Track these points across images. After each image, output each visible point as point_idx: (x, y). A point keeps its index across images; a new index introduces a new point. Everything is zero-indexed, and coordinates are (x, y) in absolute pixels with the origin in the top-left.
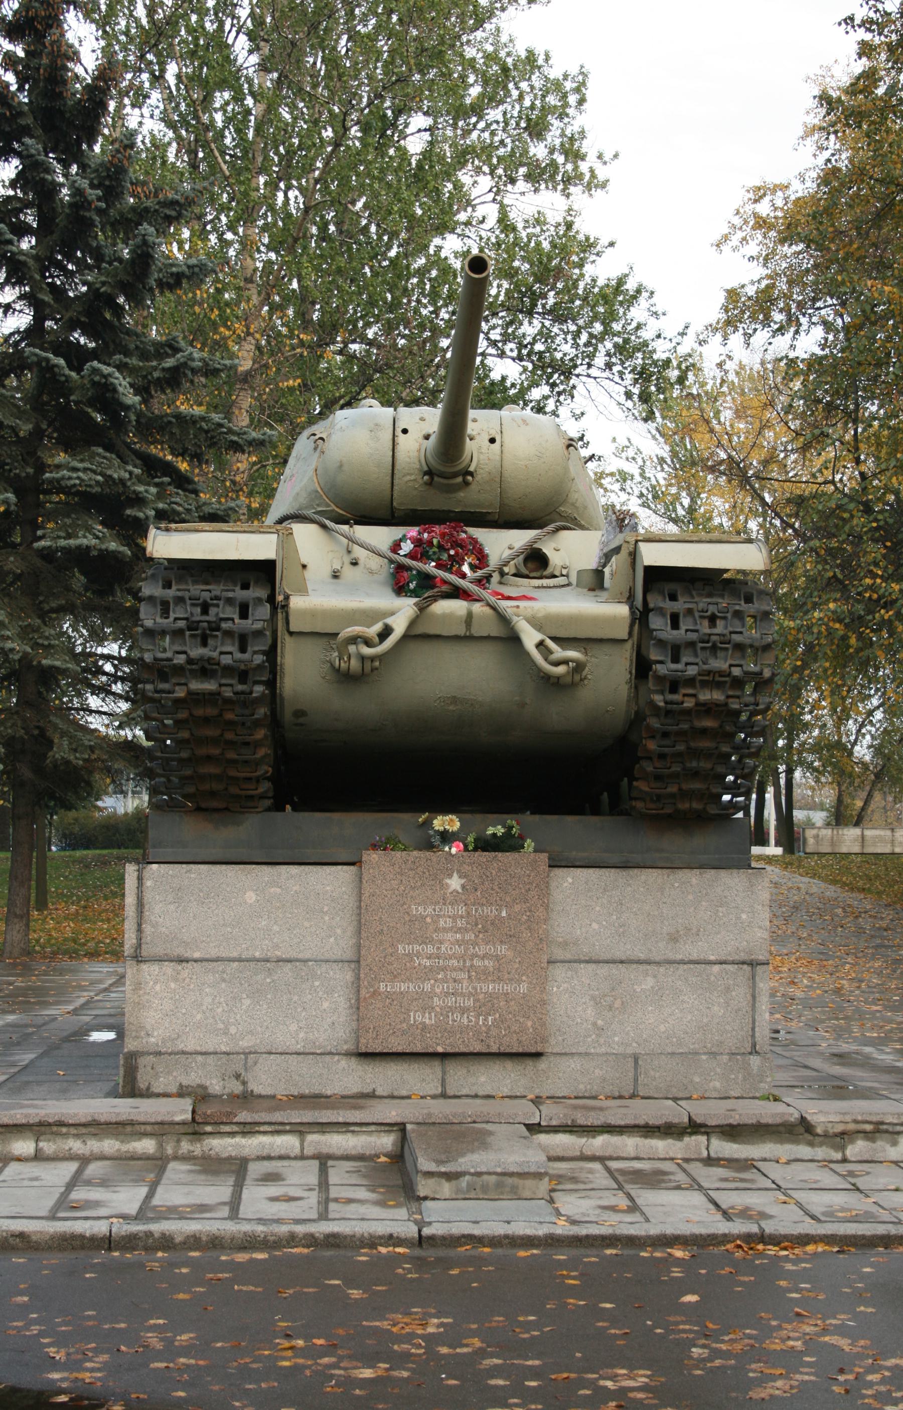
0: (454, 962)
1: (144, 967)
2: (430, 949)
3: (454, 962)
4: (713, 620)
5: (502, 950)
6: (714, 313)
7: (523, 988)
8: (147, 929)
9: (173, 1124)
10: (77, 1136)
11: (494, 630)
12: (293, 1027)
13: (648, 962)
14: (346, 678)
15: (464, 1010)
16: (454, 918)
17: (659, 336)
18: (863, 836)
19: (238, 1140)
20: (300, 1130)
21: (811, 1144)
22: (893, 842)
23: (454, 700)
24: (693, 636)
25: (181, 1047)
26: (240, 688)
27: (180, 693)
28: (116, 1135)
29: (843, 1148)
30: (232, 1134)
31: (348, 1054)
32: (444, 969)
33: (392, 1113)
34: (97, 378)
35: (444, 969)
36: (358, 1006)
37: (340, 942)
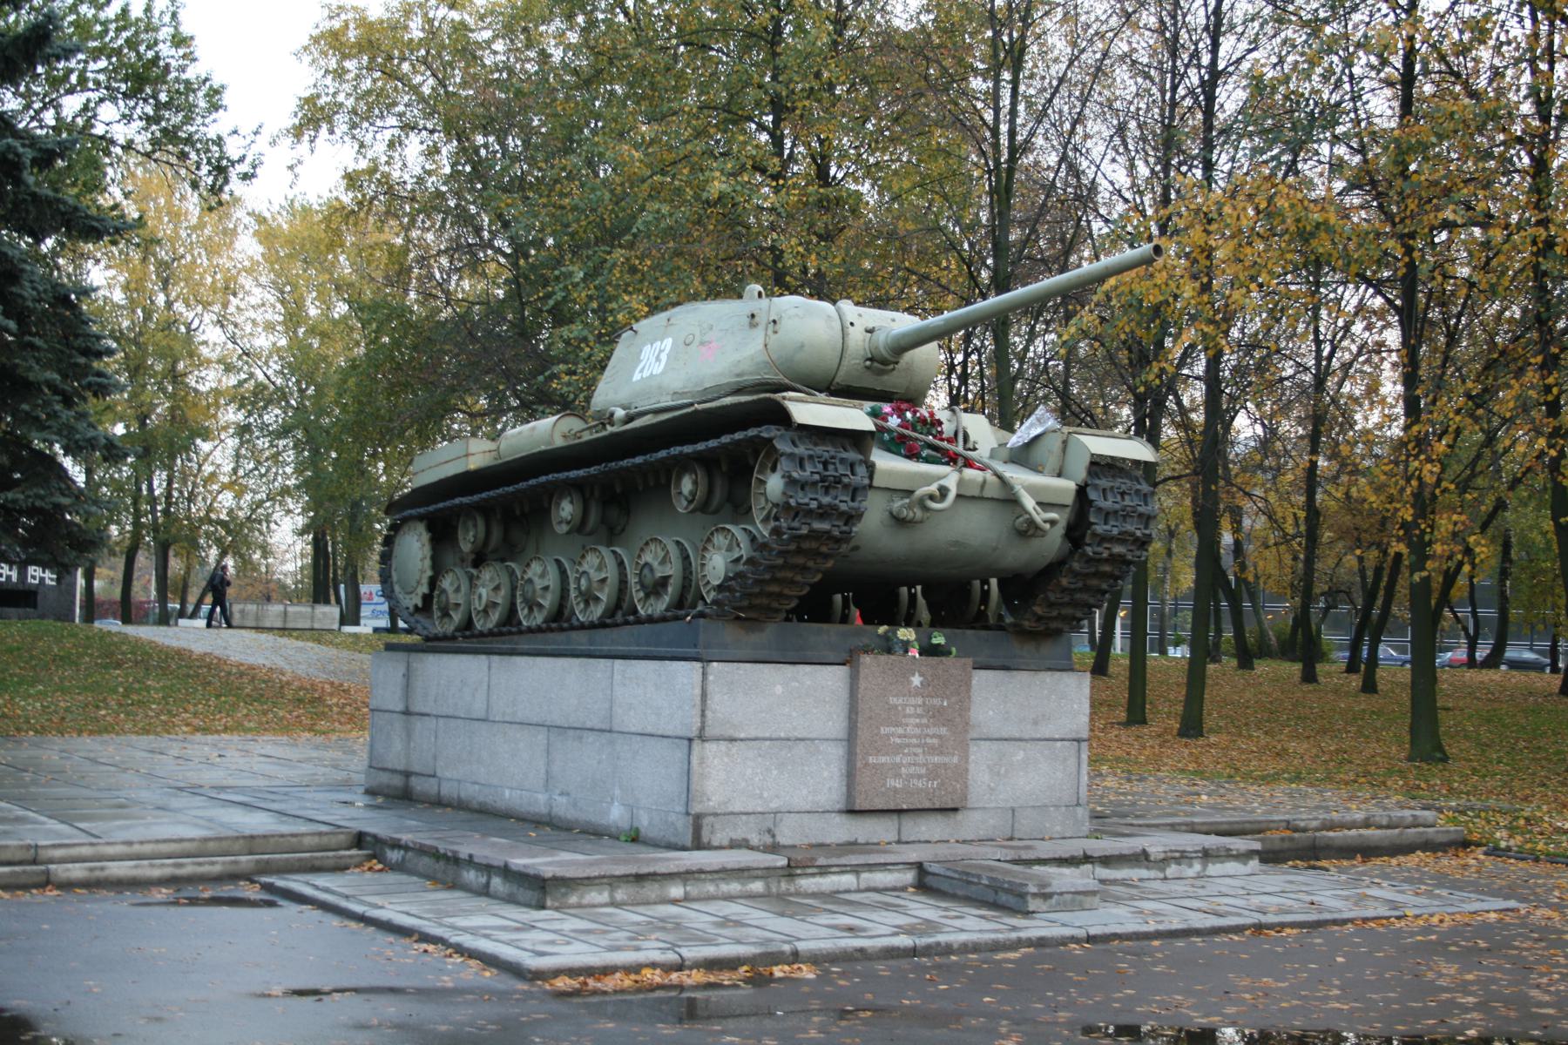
0: (914, 741)
1: (707, 745)
2: (900, 731)
3: (914, 741)
4: (1123, 494)
5: (943, 731)
6: (287, 118)
7: (955, 760)
8: (709, 714)
9: (775, 868)
10: (712, 880)
11: (993, 491)
12: (805, 792)
13: (1020, 740)
14: (899, 522)
15: (920, 777)
16: (915, 706)
17: (235, 132)
18: (285, 613)
19: (818, 879)
20: (856, 870)
21: (1148, 868)
22: (312, 618)
23: (956, 543)
24: (1117, 506)
25: (731, 809)
26: (845, 528)
27: (804, 531)
28: (738, 879)
29: (1163, 870)
30: (813, 875)
31: (840, 812)
32: (908, 746)
33: (913, 855)
34: (11, 156)
35: (908, 746)
36: (851, 776)
37: (836, 724)
